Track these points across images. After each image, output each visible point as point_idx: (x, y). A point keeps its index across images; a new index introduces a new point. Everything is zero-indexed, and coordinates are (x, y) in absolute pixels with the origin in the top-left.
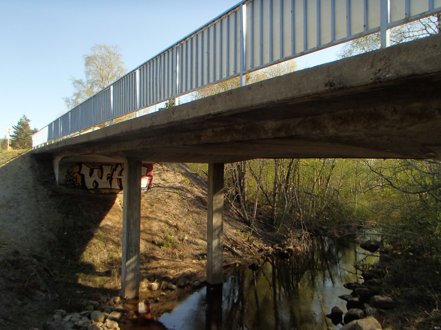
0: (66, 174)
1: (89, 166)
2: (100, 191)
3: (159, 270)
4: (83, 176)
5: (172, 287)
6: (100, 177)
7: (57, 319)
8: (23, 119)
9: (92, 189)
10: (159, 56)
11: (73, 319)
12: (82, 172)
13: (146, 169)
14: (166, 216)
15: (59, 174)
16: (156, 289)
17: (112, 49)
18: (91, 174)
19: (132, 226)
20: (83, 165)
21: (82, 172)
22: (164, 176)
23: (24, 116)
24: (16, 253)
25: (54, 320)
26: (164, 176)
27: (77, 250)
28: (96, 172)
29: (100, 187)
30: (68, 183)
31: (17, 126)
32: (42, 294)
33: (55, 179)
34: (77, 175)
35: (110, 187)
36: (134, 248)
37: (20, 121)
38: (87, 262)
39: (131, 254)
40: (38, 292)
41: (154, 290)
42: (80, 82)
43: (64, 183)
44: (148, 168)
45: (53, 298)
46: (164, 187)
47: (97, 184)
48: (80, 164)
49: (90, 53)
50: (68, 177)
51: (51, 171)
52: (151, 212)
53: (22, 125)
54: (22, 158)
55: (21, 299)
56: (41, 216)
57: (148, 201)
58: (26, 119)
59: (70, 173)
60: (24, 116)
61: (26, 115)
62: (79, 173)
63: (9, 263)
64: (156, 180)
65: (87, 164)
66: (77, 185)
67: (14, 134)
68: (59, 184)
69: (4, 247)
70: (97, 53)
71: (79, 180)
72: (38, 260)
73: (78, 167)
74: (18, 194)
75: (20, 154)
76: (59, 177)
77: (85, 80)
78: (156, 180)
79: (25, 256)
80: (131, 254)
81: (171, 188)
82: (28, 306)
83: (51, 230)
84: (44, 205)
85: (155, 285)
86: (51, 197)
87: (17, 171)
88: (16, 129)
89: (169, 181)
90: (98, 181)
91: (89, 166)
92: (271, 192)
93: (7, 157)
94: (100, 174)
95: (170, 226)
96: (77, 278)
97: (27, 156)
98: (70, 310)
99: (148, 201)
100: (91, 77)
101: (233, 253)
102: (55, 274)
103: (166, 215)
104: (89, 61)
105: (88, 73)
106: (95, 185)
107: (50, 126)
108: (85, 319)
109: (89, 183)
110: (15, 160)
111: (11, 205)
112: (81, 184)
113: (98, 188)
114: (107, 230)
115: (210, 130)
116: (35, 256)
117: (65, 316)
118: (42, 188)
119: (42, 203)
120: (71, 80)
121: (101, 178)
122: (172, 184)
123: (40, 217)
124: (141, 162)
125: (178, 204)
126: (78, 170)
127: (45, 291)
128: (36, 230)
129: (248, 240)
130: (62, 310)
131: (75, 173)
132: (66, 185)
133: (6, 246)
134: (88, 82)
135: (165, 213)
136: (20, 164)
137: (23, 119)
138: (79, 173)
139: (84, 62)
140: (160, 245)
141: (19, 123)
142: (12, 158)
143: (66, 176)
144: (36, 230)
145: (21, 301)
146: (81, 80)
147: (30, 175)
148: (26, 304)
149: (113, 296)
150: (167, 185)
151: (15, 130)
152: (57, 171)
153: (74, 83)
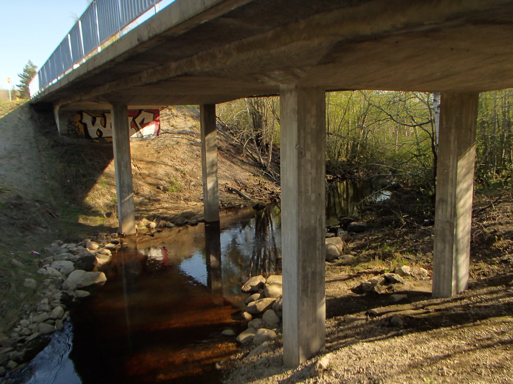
0: (68, 124)
1: (91, 114)
2: (105, 140)
3: (161, 211)
4: (85, 125)
5: (169, 224)
6: (103, 125)
7: (54, 246)
9: (96, 139)
11: (68, 247)
12: (84, 121)
13: (153, 115)
14: (173, 163)
15: (60, 124)
16: (154, 227)
18: (93, 123)
19: (123, 168)
20: (84, 114)
21: (84, 121)
22: (173, 122)
23: (30, 62)
24: (19, 197)
25: (51, 246)
26: (173, 122)
27: (80, 196)
28: (98, 120)
29: (104, 135)
30: (70, 132)
31: (23, 74)
32: (42, 229)
33: (57, 129)
34: (78, 124)
36: (127, 188)
37: (25, 69)
39: (124, 194)
40: (40, 228)
41: (152, 228)
43: (66, 133)
44: (154, 114)
45: (53, 233)
46: (173, 133)
47: (101, 133)
48: (81, 113)
50: (69, 126)
51: (53, 122)
52: (158, 158)
53: (28, 73)
54: (22, 108)
55: (22, 232)
56: (43, 165)
57: (155, 148)
58: (32, 65)
59: (71, 122)
60: (30, 62)
61: (32, 61)
62: (81, 121)
63: (12, 205)
64: (164, 126)
65: (88, 112)
66: (80, 134)
67: (21, 84)
68: (62, 134)
69: (6, 193)
71: (82, 130)
72: (40, 204)
73: (79, 116)
74: (19, 145)
75: (18, 105)
76: (60, 127)
78: (164, 126)
79: (27, 200)
80: (124, 194)
81: (179, 133)
82: (29, 237)
83: (53, 178)
84: (46, 156)
85: (153, 224)
86: (53, 147)
87: (16, 122)
88: (22, 78)
89: (179, 127)
90: (102, 130)
91: (91, 114)
93: (6, 108)
94: (103, 122)
95: (177, 170)
96: (78, 219)
97: (26, 107)
98: (68, 241)
99: (155, 148)
101: (241, 195)
102: (57, 216)
103: (173, 161)
106: (99, 134)
108: (81, 248)
109: (93, 132)
110: (14, 111)
111: (12, 155)
112: (84, 133)
113: (102, 137)
114: (108, 176)
115: (145, 72)
116: (37, 201)
117: (62, 245)
118: (43, 138)
119: (44, 153)
121: (105, 126)
122: (181, 130)
123: (42, 166)
124: (126, 107)
125: (186, 150)
126: (80, 119)
127: (46, 228)
128: (39, 178)
129: (260, 183)
130: (59, 241)
131: (76, 122)
132: (69, 135)
133: (8, 192)
135: (172, 160)
136: (19, 115)
138: (81, 121)
140: (165, 190)
141: (25, 71)
142: (10, 110)
143: (68, 125)
144: (39, 178)
145: (22, 233)
147: (30, 126)
148: (27, 236)
150: (176, 130)
151: (22, 79)
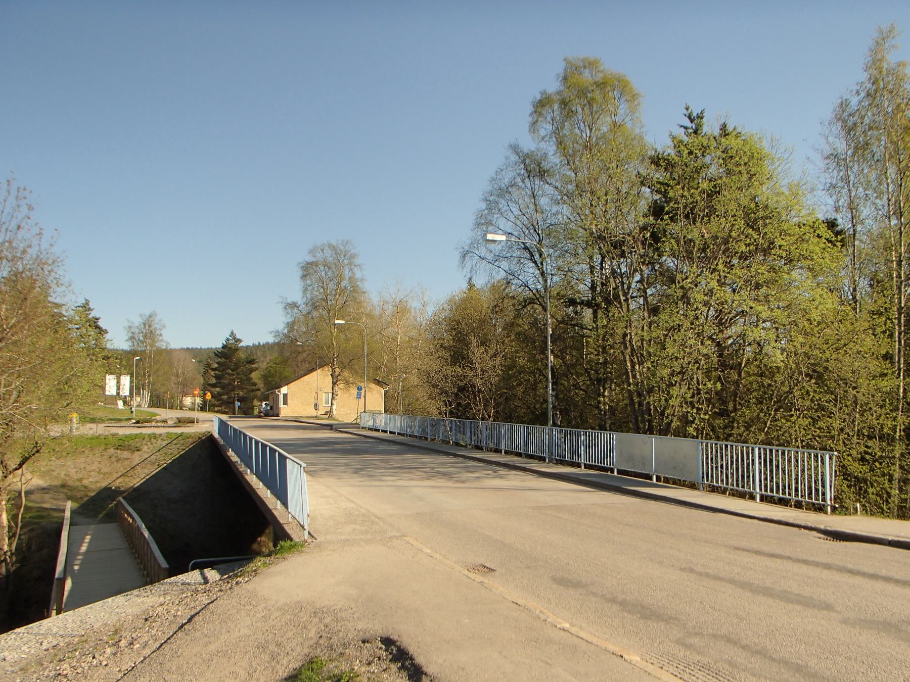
8: (231, 338)
17: (342, 247)
23: (232, 333)
37: (225, 343)
42: (294, 305)
49: (310, 259)
58: (235, 338)
60: (232, 333)
75: (199, 438)
92: (743, 257)
104: (308, 270)
105: (305, 290)
107: (51, 617)
120: (282, 303)
137: (231, 338)
139: (300, 273)
142: (191, 444)
149: (216, 569)
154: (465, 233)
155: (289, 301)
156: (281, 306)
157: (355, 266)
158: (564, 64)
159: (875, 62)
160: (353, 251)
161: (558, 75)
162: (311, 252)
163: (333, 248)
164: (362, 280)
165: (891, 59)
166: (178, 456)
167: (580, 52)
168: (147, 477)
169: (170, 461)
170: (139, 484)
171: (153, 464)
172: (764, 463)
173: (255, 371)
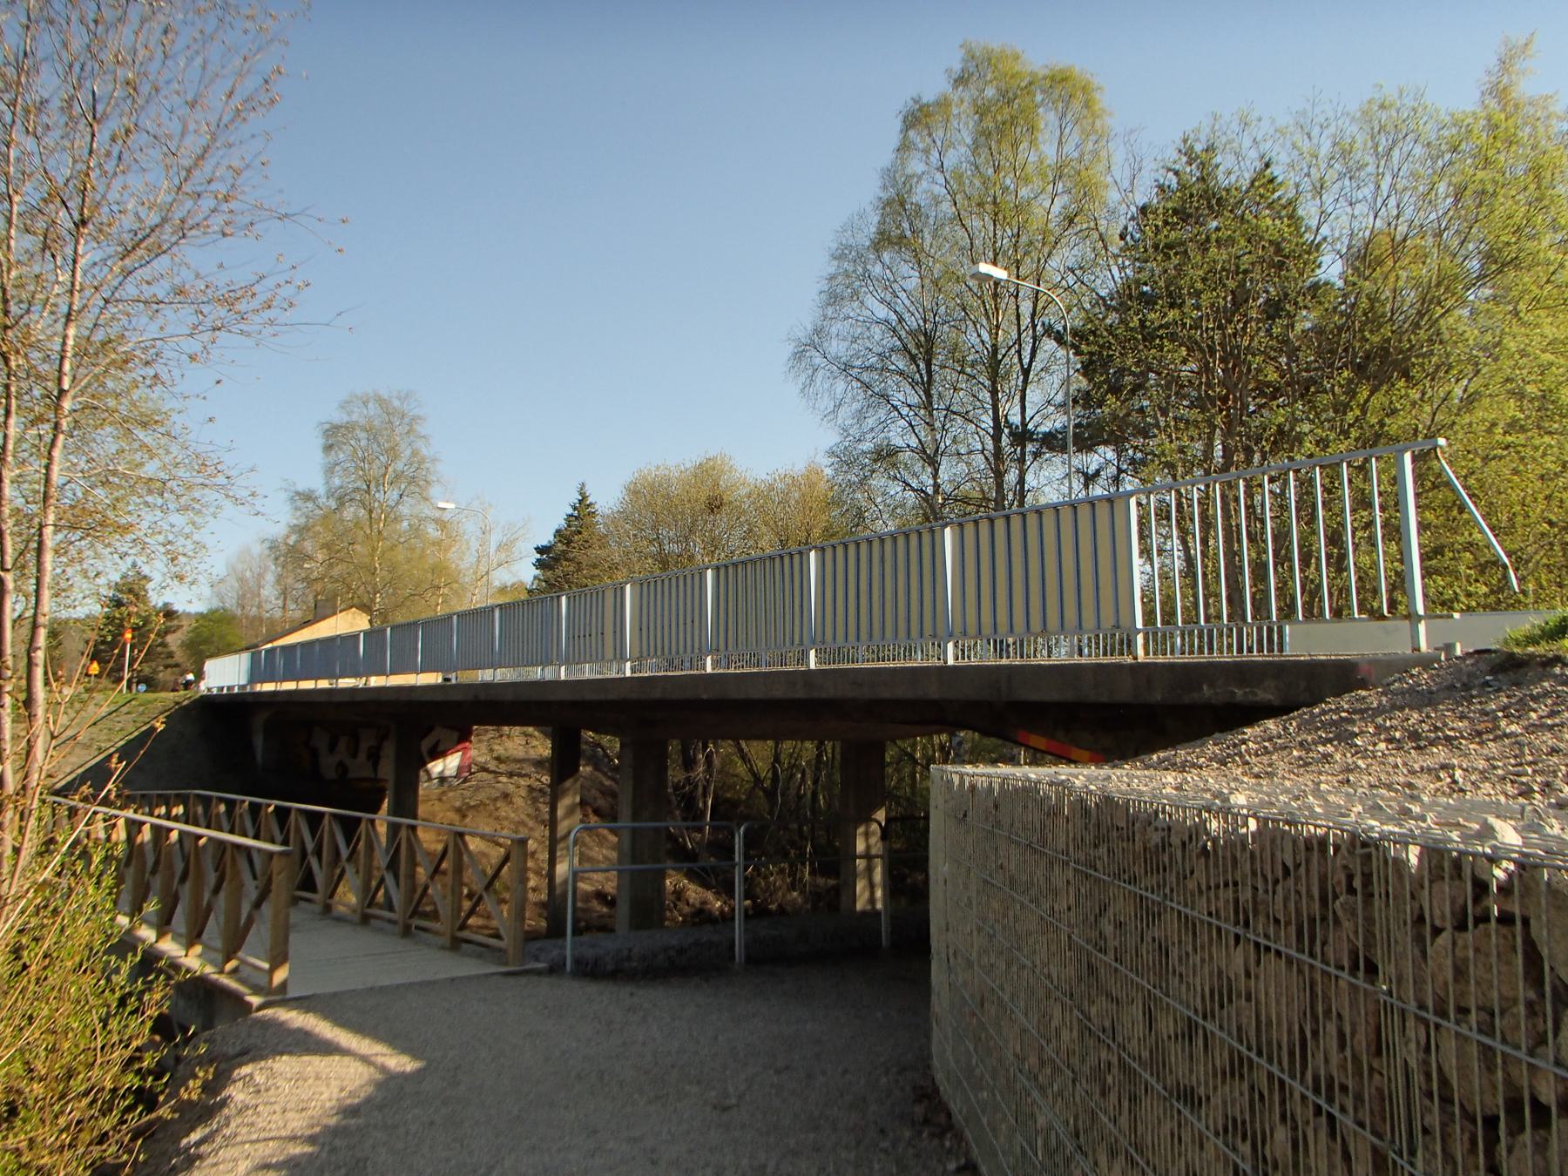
10: (420, 909)
17: (396, 403)
18: (332, 748)
28: (342, 744)
29: (351, 775)
35: (373, 776)
38: (1374, 319)
42: (308, 497)
49: (339, 417)
70: (355, 417)
75: (177, 703)
77: (321, 490)
100: (337, 481)
104: (334, 437)
105: (330, 471)
134: (330, 494)
139: (321, 441)
146: (313, 491)
152: (259, 742)
153: (292, 499)
154: (802, 311)
155: (300, 488)
156: (284, 496)
157: (1042, 163)
158: (961, 53)
159: (1499, 92)
160: (416, 412)
161: (948, 71)
162: (345, 405)
163: (381, 401)
164: (434, 460)
165: (1526, 87)
166: (136, 734)
167: (992, 38)
168: (80, 771)
169: (122, 743)
170: (63, 783)
171: (87, 747)
172: (1301, 1057)
173: (174, 632)
